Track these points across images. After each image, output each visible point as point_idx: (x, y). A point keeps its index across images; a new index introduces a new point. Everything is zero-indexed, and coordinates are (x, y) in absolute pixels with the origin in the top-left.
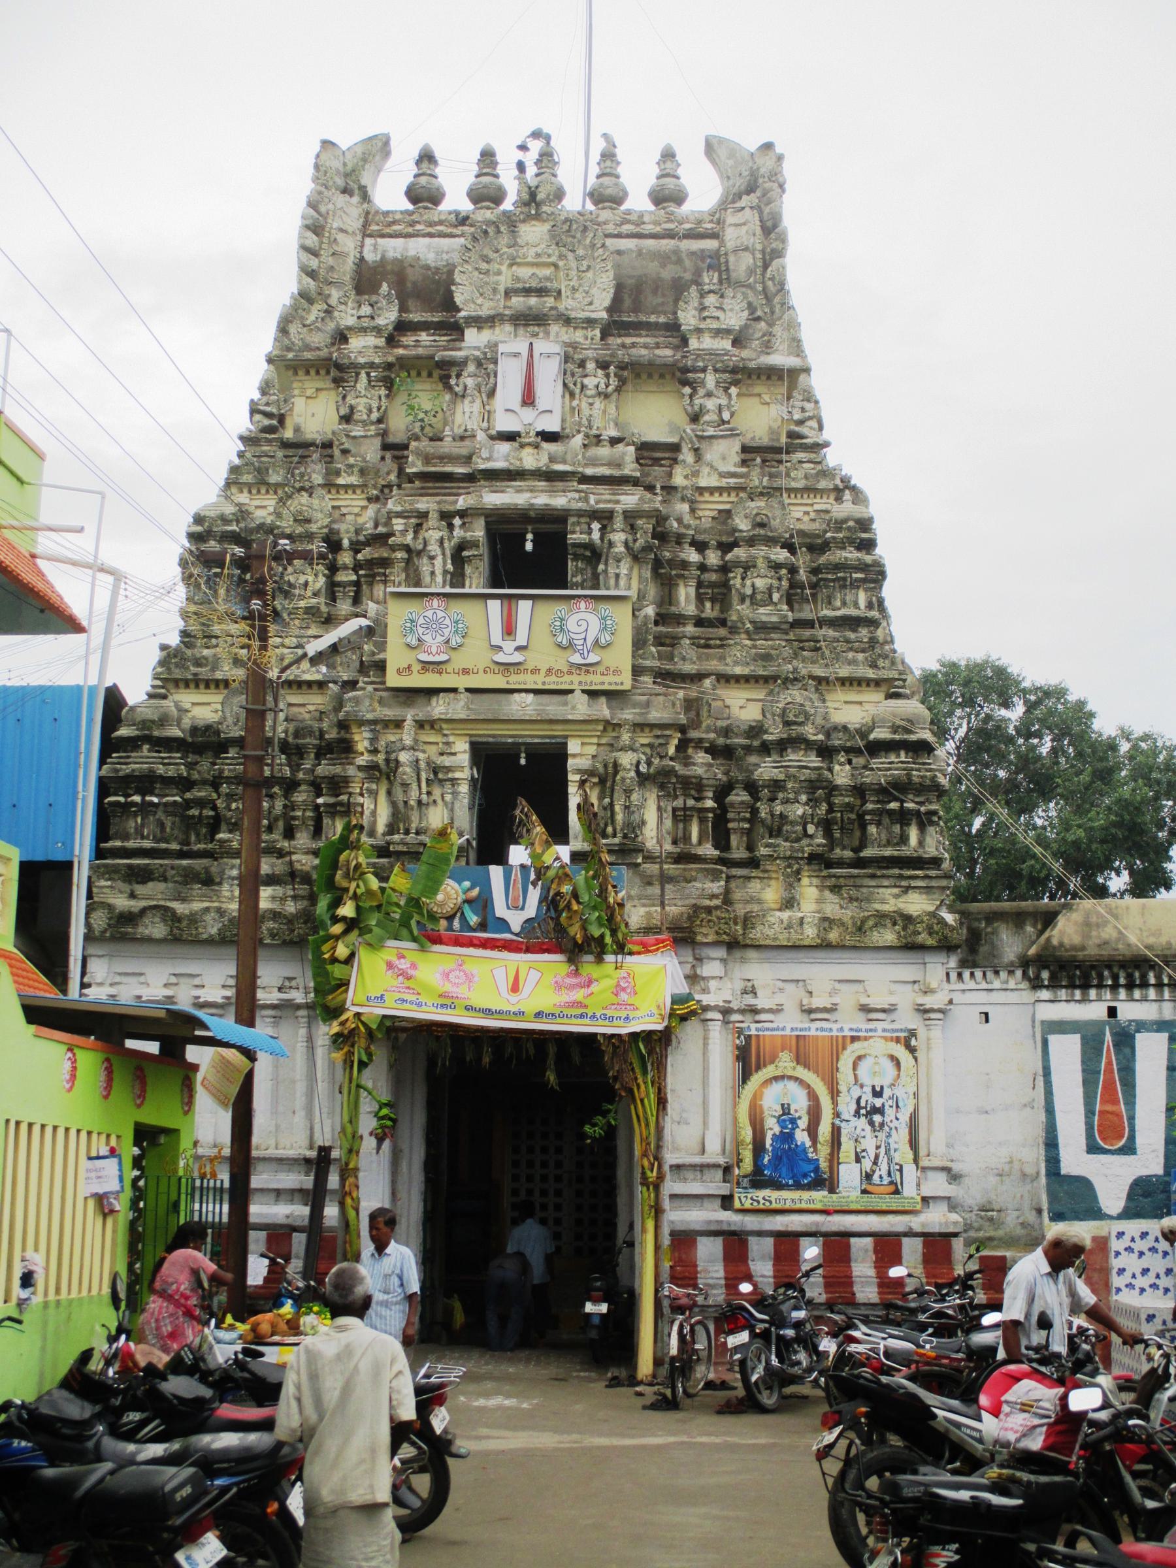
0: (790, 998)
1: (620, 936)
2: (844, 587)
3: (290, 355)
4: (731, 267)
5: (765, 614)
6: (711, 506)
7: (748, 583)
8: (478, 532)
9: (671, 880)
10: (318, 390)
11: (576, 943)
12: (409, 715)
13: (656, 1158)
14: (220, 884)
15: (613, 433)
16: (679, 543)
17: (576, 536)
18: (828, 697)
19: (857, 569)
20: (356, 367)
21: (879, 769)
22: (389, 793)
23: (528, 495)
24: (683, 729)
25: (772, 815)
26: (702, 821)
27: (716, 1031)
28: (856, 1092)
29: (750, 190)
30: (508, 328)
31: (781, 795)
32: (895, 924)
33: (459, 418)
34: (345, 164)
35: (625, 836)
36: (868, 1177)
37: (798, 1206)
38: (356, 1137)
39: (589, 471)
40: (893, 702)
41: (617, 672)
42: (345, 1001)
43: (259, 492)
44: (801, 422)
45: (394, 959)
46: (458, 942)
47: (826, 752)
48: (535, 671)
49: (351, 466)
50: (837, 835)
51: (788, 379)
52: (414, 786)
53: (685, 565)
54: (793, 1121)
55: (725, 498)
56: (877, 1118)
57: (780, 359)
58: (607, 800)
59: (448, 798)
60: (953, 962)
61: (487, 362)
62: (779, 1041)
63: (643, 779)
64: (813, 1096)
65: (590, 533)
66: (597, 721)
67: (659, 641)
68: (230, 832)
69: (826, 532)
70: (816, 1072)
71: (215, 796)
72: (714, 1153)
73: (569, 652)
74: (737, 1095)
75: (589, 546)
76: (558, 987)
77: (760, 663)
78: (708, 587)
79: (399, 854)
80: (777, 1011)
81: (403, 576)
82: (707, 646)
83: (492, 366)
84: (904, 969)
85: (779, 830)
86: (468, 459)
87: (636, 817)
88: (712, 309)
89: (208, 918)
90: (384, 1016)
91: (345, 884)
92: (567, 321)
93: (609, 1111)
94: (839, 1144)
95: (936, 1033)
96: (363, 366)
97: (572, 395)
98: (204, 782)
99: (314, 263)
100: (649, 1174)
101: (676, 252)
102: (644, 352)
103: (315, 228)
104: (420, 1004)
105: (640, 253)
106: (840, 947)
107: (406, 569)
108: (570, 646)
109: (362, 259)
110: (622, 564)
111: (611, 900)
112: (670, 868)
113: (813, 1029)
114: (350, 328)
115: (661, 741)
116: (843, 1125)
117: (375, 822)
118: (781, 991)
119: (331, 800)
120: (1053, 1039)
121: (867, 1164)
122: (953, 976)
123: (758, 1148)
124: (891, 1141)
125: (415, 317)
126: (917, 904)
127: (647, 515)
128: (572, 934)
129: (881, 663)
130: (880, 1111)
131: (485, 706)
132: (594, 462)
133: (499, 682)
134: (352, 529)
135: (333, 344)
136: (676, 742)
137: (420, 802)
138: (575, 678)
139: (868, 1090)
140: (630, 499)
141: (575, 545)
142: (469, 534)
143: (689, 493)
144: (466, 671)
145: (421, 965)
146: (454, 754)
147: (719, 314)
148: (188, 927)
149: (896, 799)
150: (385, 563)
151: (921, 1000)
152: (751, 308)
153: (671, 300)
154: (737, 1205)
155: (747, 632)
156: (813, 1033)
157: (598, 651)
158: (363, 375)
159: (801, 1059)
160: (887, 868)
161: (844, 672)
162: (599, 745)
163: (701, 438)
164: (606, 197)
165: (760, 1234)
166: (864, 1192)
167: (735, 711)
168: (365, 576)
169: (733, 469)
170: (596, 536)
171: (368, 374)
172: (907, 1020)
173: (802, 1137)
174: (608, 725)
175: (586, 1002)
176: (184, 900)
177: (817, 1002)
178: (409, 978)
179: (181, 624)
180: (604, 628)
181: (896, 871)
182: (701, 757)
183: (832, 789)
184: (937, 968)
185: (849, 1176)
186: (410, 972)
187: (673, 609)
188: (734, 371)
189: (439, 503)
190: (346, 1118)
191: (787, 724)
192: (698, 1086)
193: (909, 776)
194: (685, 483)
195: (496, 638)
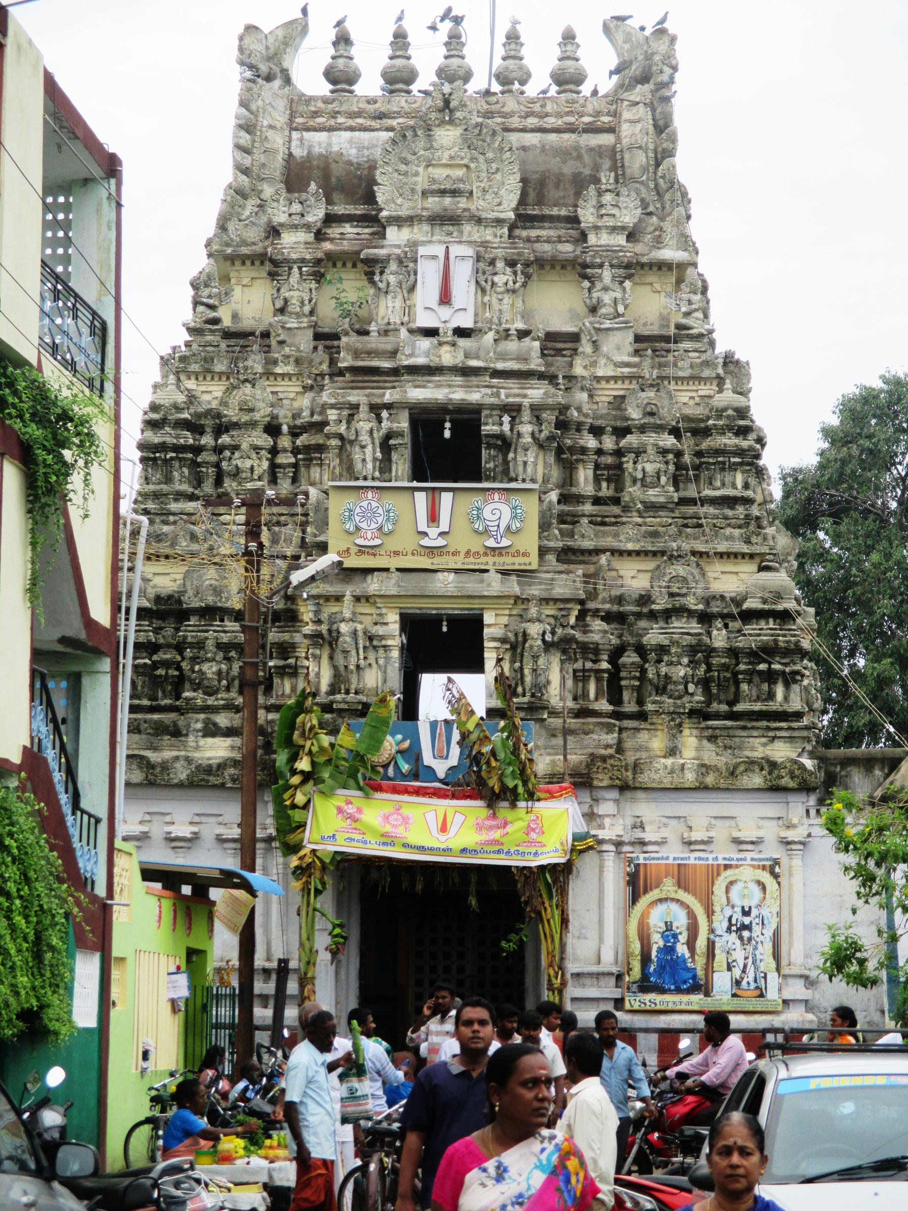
0: (672, 832)
1: (530, 786)
2: (723, 469)
3: (229, 251)
4: (627, 164)
5: (653, 495)
6: (607, 393)
7: (639, 467)
8: (403, 424)
9: (572, 732)
10: (252, 279)
11: (494, 792)
12: (349, 591)
13: (560, 968)
14: (186, 735)
15: (520, 325)
16: (578, 430)
17: (489, 428)
18: (707, 568)
19: (735, 454)
20: (288, 263)
21: (750, 635)
22: (331, 658)
23: (446, 390)
24: (582, 602)
25: (659, 676)
26: (599, 680)
27: (610, 861)
28: (728, 912)
29: (644, 79)
30: (426, 227)
31: (666, 658)
32: (762, 769)
33: (382, 311)
34: (267, 48)
35: (533, 695)
36: (738, 983)
37: (678, 1007)
38: (313, 952)
39: (500, 366)
40: (763, 575)
41: (525, 554)
42: (302, 840)
43: (205, 378)
44: (687, 314)
45: (343, 804)
46: (395, 790)
47: (705, 618)
48: (456, 553)
49: (288, 357)
50: (715, 691)
51: (677, 272)
52: (354, 653)
53: (584, 450)
54: (675, 936)
55: (619, 385)
56: (746, 934)
57: (669, 254)
58: (517, 665)
59: (381, 662)
60: (812, 800)
61: (408, 261)
62: (663, 869)
63: (548, 646)
64: (691, 915)
65: (501, 424)
66: (509, 597)
67: (562, 519)
68: (195, 691)
69: (708, 418)
70: (695, 895)
71: (179, 658)
72: (608, 962)
73: (485, 537)
74: (628, 915)
75: (501, 436)
76: (479, 828)
77: (649, 539)
78: (604, 469)
79: (340, 711)
80: (662, 843)
81: (338, 461)
82: (603, 524)
83: (411, 265)
84: (770, 807)
85: (665, 688)
86: (394, 353)
87: (542, 679)
88: (609, 207)
89: (178, 765)
90: (336, 852)
91: (301, 742)
92: (479, 221)
93: (521, 929)
94: (714, 956)
95: (797, 862)
96: (295, 262)
97: (483, 291)
98: (169, 646)
99: (247, 161)
100: (554, 981)
101: (577, 148)
102: (547, 247)
103: (247, 127)
104: (365, 842)
105: (543, 150)
106: (716, 789)
107: (340, 455)
108: (486, 532)
109: (290, 154)
110: (529, 453)
111: (523, 757)
112: (572, 722)
113: (692, 859)
114: (282, 225)
115: (563, 613)
116: (717, 939)
117: (319, 682)
118: (664, 827)
119: (281, 663)
121: (737, 972)
122: (813, 812)
123: (646, 959)
124: (757, 952)
125: (340, 209)
126: (781, 752)
127: (551, 408)
128: (491, 785)
129: (754, 539)
130: (748, 927)
132: (503, 357)
134: (290, 415)
135: (267, 238)
136: (576, 613)
137: (358, 667)
138: (490, 559)
139: (738, 910)
140: (536, 393)
141: (487, 436)
142: (395, 425)
143: (587, 383)
144: (396, 553)
145: (366, 810)
146: (386, 624)
147: (615, 211)
148: (161, 772)
149: (765, 661)
151: (784, 834)
152: (644, 204)
153: (571, 192)
154: (627, 1006)
155: (638, 511)
156: (692, 861)
157: (509, 536)
158: (295, 270)
159: (681, 884)
160: (757, 720)
161: (722, 547)
162: (510, 615)
163: (598, 330)
164: (510, 78)
165: (647, 1030)
166: (734, 995)
167: (628, 582)
168: (303, 460)
169: (626, 359)
170: (506, 428)
171: (300, 268)
172: (772, 851)
173: (682, 949)
175: (503, 840)
176: (155, 749)
177: (696, 836)
178: (356, 821)
180: (514, 517)
181: (764, 723)
182: (597, 625)
183: (710, 651)
184: (797, 807)
185: (722, 982)
186: (357, 816)
187: (574, 490)
188: (628, 266)
189: (367, 396)
190: (304, 936)
191: (672, 595)
192: (594, 906)
193: (776, 641)
194: (585, 373)
195: (423, 526)
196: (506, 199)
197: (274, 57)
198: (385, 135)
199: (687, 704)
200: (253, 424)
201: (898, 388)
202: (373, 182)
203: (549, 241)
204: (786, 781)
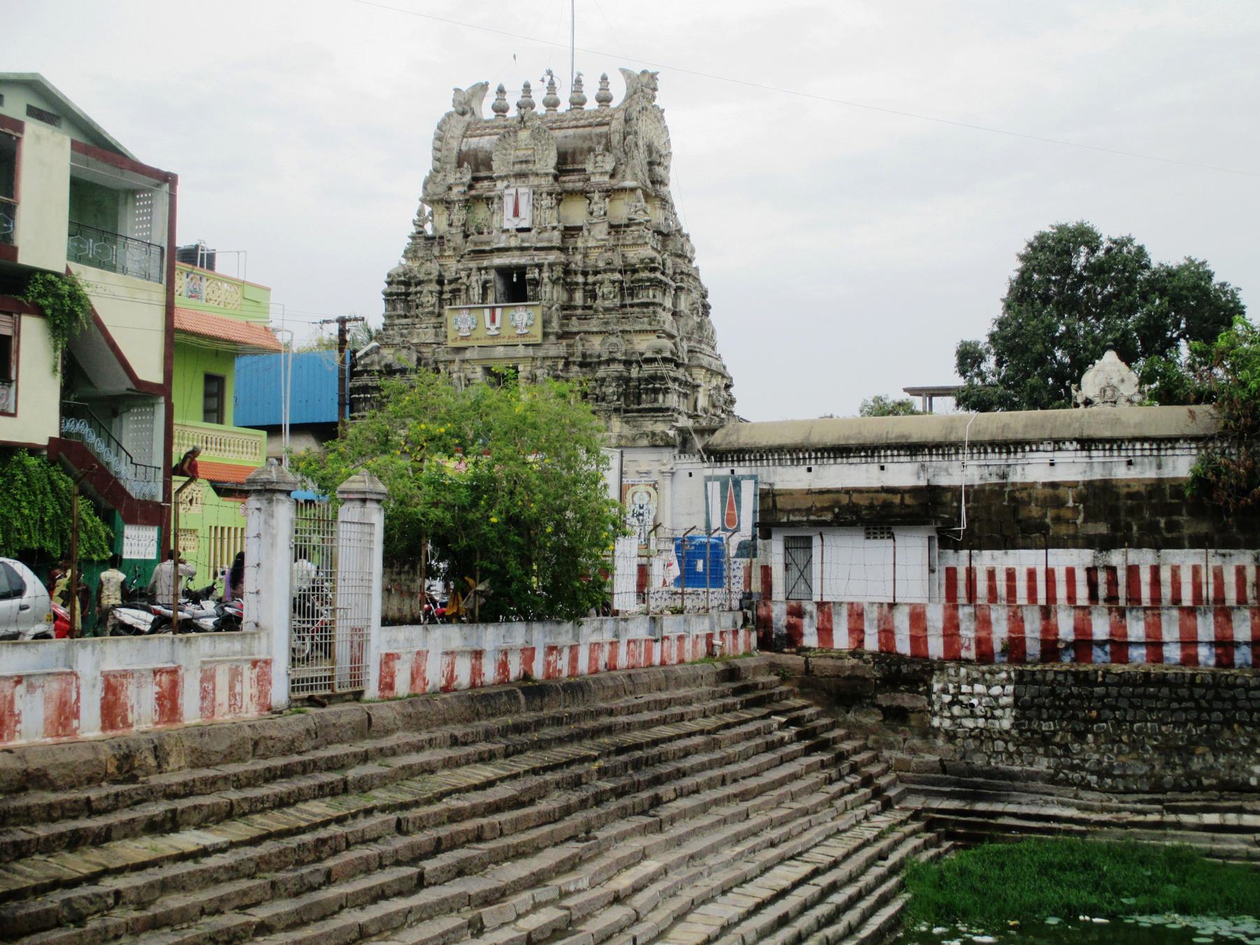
5: (608, 304)
12: (457, 358)
20: (453, 202)
39: (539, 245)
47: (628, 363)
53: (577, 284)
75: (534, 279)
84: (653, 455)
92: (537, 175)
120: (709, 484)
126: (660, 427)
131: (485, 353)
133: (490, 342)
140: (552, 257)
150: (459, 290)
161: (637, 328)
170: (537, 275)
174: (533, 359)
179: (383, 320)
183: (630, 379)
184: (667, 456)
188: (608, 191)
196: (549, 162)
197: (468, 103)
198: (496, 137)
200: (431, 281)
202: (491, 159)
203: (573, 182)
204: (659, 442)
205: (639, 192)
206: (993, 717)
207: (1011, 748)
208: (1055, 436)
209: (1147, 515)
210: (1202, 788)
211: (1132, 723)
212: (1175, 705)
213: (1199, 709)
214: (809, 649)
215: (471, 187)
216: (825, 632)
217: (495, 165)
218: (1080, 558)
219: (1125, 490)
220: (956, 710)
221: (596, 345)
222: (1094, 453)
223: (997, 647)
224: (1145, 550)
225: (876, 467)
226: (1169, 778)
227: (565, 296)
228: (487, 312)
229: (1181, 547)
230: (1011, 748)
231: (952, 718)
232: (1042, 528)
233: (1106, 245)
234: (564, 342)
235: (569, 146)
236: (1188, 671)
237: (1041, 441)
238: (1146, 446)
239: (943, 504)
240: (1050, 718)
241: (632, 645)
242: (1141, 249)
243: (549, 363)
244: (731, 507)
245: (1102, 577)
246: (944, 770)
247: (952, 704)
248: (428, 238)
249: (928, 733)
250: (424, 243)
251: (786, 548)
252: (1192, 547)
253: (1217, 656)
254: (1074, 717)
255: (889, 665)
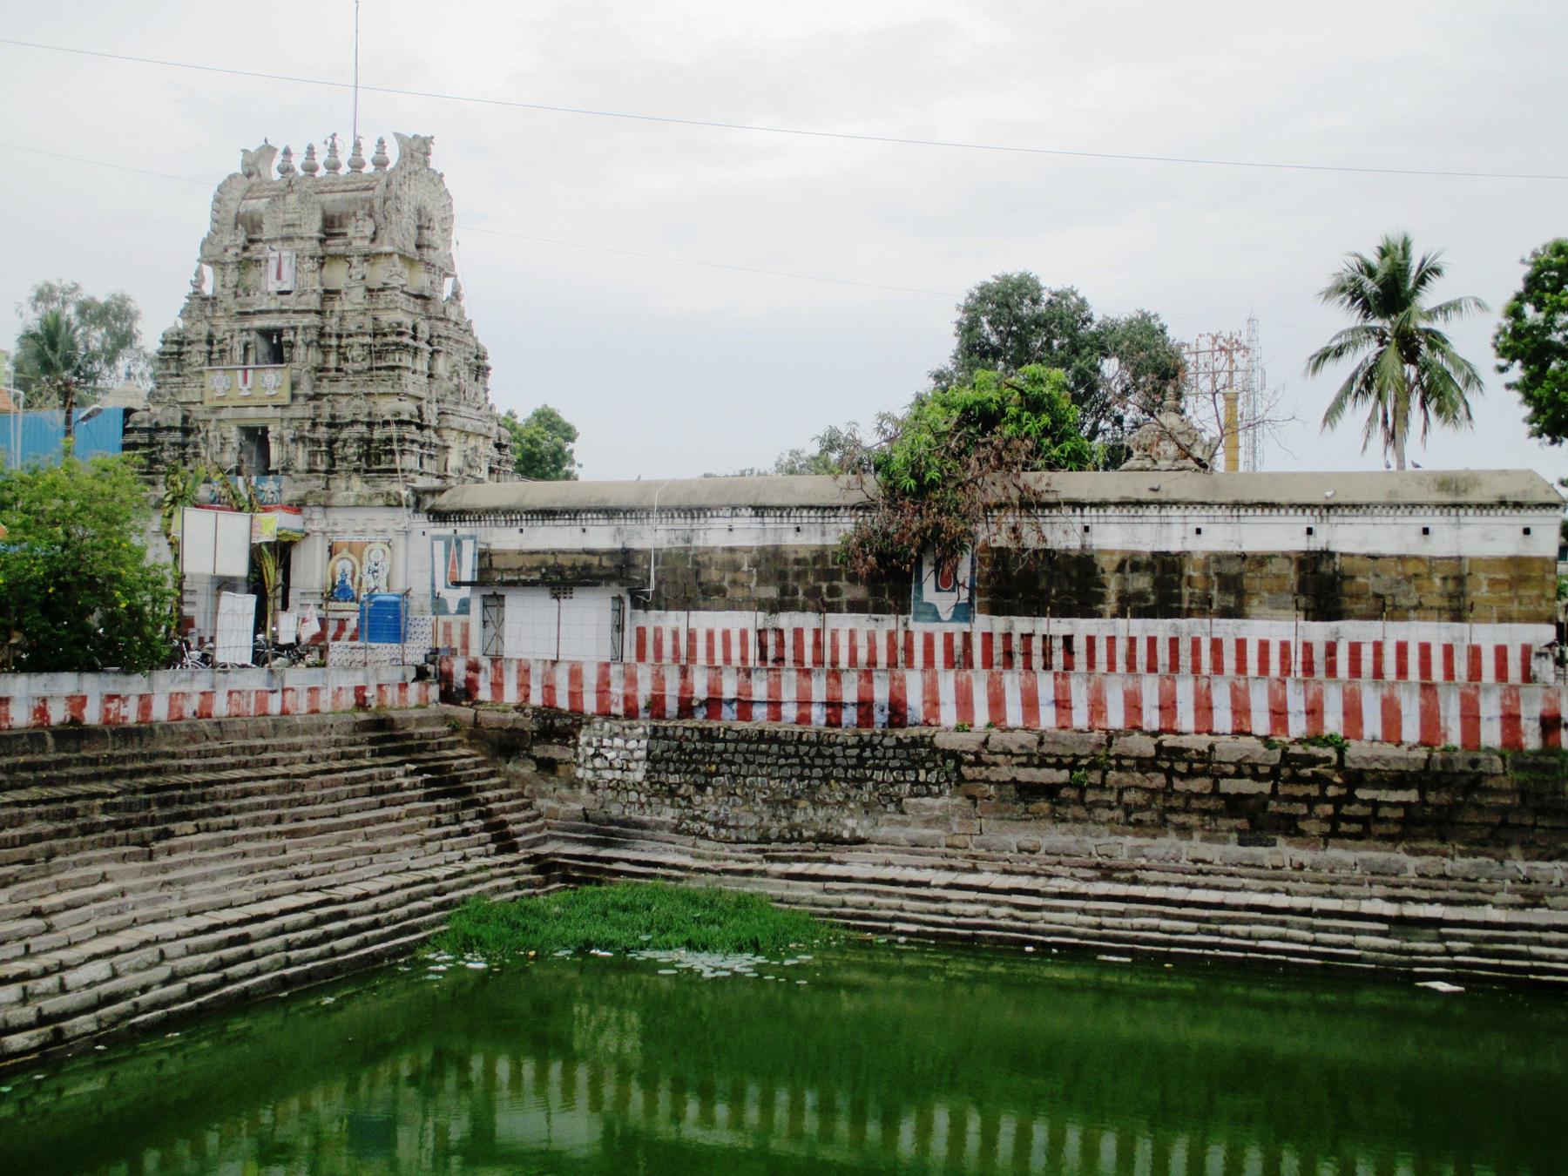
5: (357, 367)
12: (214, 417)
47: (370, 425)
84: (389, 514)
118: (347, 524)
120: (436, 543)
159: (350, 551)
173: (348, 582)
184: (403, 516)
196: (314, 227)
199: (353, 466)
201: (1559, 249)
205: (396, 257)
206: (628, 770)
207: (643, 799)
208: (733, 503)
209: (37, 598)
210: (801, 839)
211: (745, 777)
212: (782, 761)
213: (803, 765)
214: (480, 703)
215: (245, 249)
216: (497, 686)
217: (265, 227)
218: (744, 621)
219: (792, 557)
220: (598, 762)
221: (345, 410)
222: (767, 520)
223: (642, 704)
224: (809, 614)
225: (578, 530)
226: (774, 832)
227: (320, 358)
228: (240, 373)
229: (840, 611)
230: (643, 799)
231: (594, 769)
232: (720, 591)
233: (1046, 297)
234: (312, 404)
235: (334, 210)
236: (798, 729)
237: (720, 508)
238: (812, 513)
239: (634, 566)
240: (677, 771)
241: (235, 696)
242: (1083, 301)
243: (296, 423)
244: (454, 567)
245: (771, 639)
246: (587, 819)
247: (595, 756)
248: (205, 299)
249: (573, 783)
250: (200, 303)
251: (485, 606)
252: (851, 611)
253: (828, 715)
254: (696, 771)
255: (545, 719)
